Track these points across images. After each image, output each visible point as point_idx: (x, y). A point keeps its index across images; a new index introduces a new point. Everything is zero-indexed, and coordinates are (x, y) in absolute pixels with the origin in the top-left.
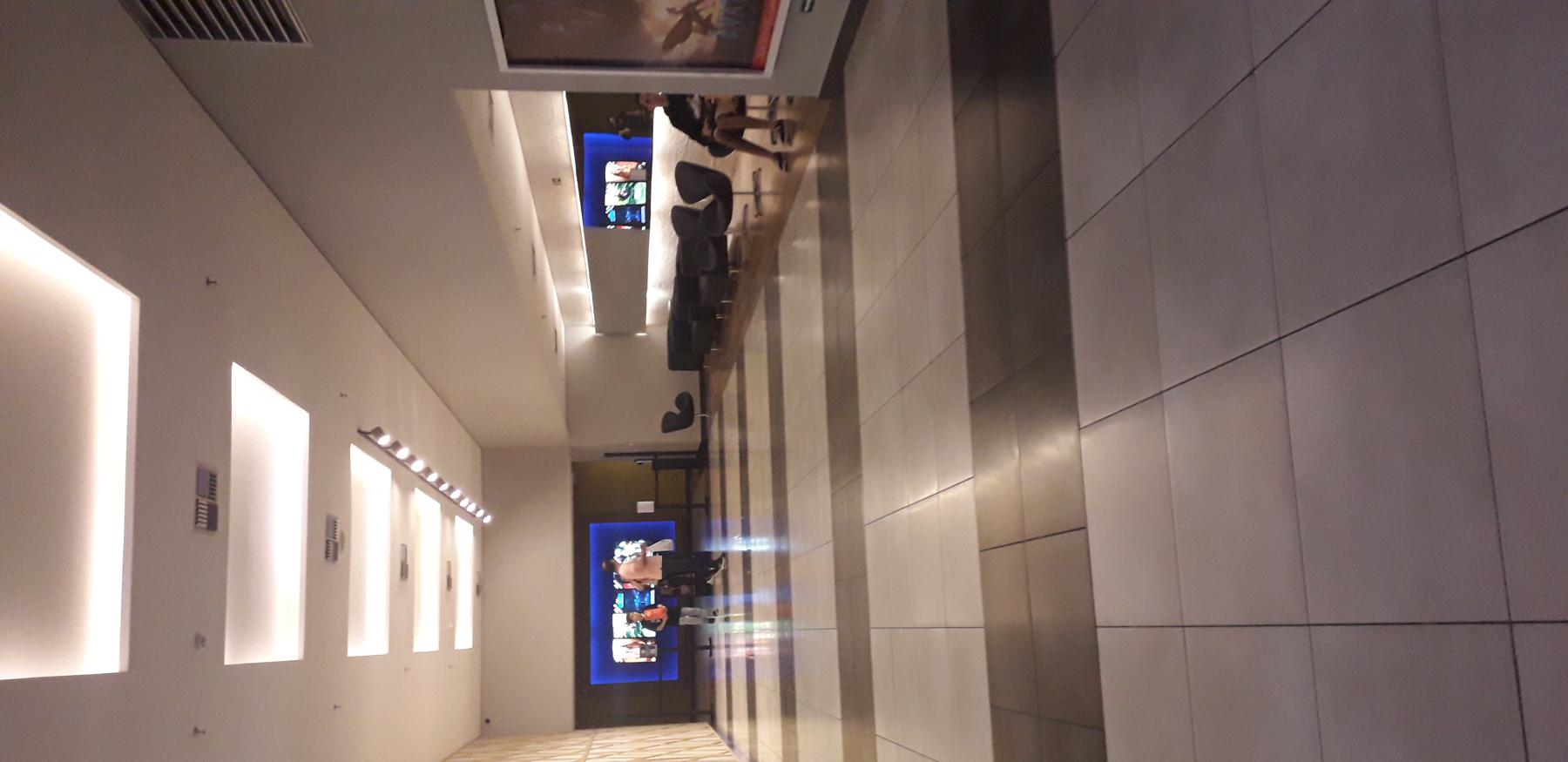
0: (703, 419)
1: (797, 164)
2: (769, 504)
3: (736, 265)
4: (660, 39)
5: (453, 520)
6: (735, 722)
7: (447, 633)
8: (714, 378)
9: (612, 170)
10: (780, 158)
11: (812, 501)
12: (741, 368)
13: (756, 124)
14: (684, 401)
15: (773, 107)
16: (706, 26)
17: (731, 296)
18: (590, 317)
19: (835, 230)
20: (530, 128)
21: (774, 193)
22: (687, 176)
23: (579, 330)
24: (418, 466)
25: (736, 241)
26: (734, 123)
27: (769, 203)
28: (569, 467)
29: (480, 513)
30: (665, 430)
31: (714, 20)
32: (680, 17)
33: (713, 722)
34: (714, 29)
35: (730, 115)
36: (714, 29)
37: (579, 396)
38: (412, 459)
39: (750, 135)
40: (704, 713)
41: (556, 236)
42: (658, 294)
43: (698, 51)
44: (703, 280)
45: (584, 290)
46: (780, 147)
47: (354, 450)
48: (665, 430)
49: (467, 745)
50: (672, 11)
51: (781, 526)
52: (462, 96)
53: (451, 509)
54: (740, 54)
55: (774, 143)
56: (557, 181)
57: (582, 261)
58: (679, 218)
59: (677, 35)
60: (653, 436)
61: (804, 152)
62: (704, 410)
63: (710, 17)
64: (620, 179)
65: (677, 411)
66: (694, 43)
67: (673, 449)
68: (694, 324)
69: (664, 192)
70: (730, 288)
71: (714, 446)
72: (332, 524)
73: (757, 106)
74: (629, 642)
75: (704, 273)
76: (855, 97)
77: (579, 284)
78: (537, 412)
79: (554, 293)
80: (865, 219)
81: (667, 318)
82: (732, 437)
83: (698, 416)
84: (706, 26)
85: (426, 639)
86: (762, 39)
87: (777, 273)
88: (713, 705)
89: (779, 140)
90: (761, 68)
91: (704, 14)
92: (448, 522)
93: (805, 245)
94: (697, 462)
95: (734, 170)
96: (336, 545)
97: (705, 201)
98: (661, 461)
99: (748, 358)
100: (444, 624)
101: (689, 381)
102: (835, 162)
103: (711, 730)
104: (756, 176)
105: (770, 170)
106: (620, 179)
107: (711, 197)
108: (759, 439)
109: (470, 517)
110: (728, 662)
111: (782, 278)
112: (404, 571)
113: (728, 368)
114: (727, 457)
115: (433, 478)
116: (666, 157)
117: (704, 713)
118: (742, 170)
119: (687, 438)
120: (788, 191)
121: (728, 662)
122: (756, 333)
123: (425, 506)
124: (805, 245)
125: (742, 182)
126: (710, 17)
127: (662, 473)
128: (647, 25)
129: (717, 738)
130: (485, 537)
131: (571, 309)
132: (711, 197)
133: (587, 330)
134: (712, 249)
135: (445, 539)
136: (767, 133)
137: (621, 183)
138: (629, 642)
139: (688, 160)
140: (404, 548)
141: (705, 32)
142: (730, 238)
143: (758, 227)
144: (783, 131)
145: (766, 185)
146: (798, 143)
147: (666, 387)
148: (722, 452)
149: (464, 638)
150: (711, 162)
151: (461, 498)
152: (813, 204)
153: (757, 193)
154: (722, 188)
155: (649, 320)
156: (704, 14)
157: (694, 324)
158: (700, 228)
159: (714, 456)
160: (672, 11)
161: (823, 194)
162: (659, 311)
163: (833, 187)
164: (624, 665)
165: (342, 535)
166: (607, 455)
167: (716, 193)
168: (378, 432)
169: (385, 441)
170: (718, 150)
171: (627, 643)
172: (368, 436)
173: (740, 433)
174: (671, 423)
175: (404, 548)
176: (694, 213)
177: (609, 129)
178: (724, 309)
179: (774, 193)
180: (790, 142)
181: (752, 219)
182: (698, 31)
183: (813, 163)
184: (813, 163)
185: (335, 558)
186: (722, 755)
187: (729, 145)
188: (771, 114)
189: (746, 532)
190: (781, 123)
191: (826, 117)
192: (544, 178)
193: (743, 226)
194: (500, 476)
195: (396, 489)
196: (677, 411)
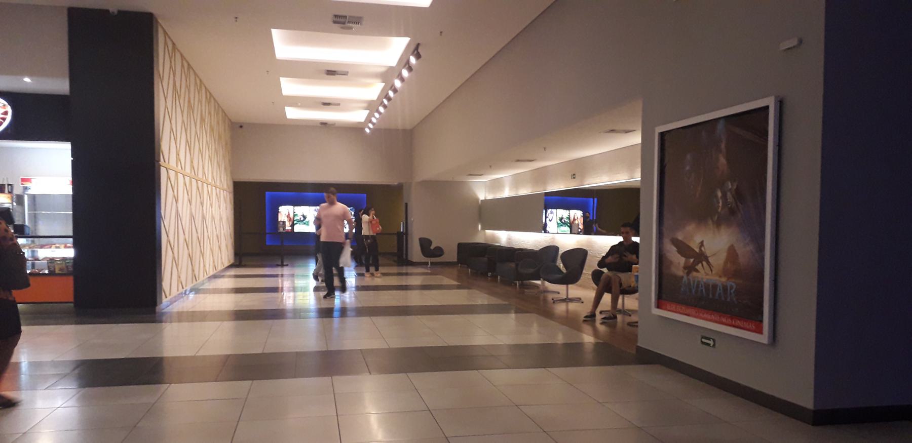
0: (427, 264)
1: (587, 328)
2: (394, 303)
3: (522, 286)
4: (680, 236)
5: (366, 109)
6: (233, 280)
7: (297, 102)
8: (454, 271)
9: (577, 214)
10: (591, 317)
11: (358, 336)
12: (459, 287)
13: (615, 301)
14: (439, 252)
15: (625, 312)
16: (690, 269)
17: (503, 282)
18: (490, 197)
19: (544, 356)
20: (614, 158)
21: (567, 311)
22: (578, 256)
23: (483, 189)
24: (398, 84)
25: (537, 286)
26: (615, 288)
27: (560, 308)
28: (402, 181)
29: (371, 126)
30: (420, 239)
31: (694, 274)
32: (697, 250)
33: (231, 266)
34: (688, 274)
35: (621, 285)
36: (688, 274)
37: (446, 191)
38: (402, 79)
39: (607, 298)
40: (241, 262)
41: (541, 175)
42: (503, 237)
43: (671, 262)
44: (513, 265)
45: (507, 193)
46: (599, 317)
47: (406, 40)
48: (420, 239)
49: (225, 114)
50: (702, 244)
51: (362, 312)
52: (638, 106)
53: (371, 106)
54: (669, 292)
55: (601, 312)
56: (574, 176)
57: (524, 191)
58: (551, 250)
59: (683, 249)
60: (417, 233)
61: (596, 333)
62: (432, 263)
63: (697, 271)
64: (572, 218)
65: (432, 248)
66: (678, 261)
67: (409, 246)
68: (485, 259)
69: (568, 241)
70: (508, 282)
71: (411, 269)
72: (357, 21)
73: (630, 302)
74: (292, 216)
75: (517, 265)
76: (638, 373)
77: (510, 190)
78: (433, 165)
79: (505, 175)
80: (554, 382)
81: (490, 243)
82: (416, 281)
83: (429, 260)
84: (690, 269)
85: (289, 87)
86: (692, 311)
87: (516, 312)
88: (245, 266)
89: (603, 316)
90: (659, 306)
91: (699, 267)
92: (365, 105)
93: (535, 332)
94: (402, 259)
95: (580, 286)
96: (344, 23)
97: (561, 266)
98: (402, 238)
99: (464, 292)
100: (300, 100)
101: (451, 255)
102: (589, 356)
103: (227, 264)
104: (578, 300)
105: (584, 310)
106: (572, 218)
107: (564, 270)
108: (415, 298)
109: (368, 120)
110: (277, 276)
111: (513, 315)
112: (331, 73)
113: (458, 280)
114: (404, 277)
115: (391, 94)
116: (589, 243)
117: (241, 262)
118: (583, 292)
119: (415, 253)
120: (570, 321)
121: (277, 276)
122: (481, 298)
123: (373, 91)
124: (535, 332)
125: (574, 291)
126: (697, 271)
127: (395, 237)
128: (690, 227)
129: (220, 268)
130: (355, 130)
131: (496, 185)
132: (564, 270)
133: (483, 195)
134: (531, 270)
135: (355, 102)
136: (609, 308)
137: (569, 218)
138: (292, 216)
139: (588, 257)
140: (345, 74)
141: (685, 268)
142: (539, 282)
143: (545, 300)
144: (610, 319)
145: (572, 306)
146: (602, 328)
147: (448, 241)
148: (407, 274)
149: (292, 113)
150: (587, 272)
151: (380, 113)
152: (560, 339)
153: (568, 300)
154: (571, 277)
155: (488, 232)
156: (699, 267)
157: (485, 259)
158: (543, 261)
159: (404, 269)
160: (702, 244)
161: (567, 346)
162: (494, 238)
163: (571, 355)
164: (277, 212)
165: (351, 28)
166: (406, 204)
167: (566, 275)
168: (418, 57)
169: (413, 60)
170: (596, 276)
171: (301, 218)
172: (416, 50)
173: (418, 288)
174: (425, 244)
175: (345, 74)
176: (555, 260)
177: (605, 208)
178: (494, 278)
179: (567, 311)
180: (601, 324)
181: (550, 297)
182: (686, 263)
183: (588, 339)
184: (588, 339)
185: (335, 22)
186: (205, 270)
187: (601, 284)
188: (620, 311)
189: (359, 288)
190: (615, 317)
191: (621, 349)
192: (578, 168)
193: (546, 291)
194: (395, 140)
195: (383, 70)
196: (432, 248)
